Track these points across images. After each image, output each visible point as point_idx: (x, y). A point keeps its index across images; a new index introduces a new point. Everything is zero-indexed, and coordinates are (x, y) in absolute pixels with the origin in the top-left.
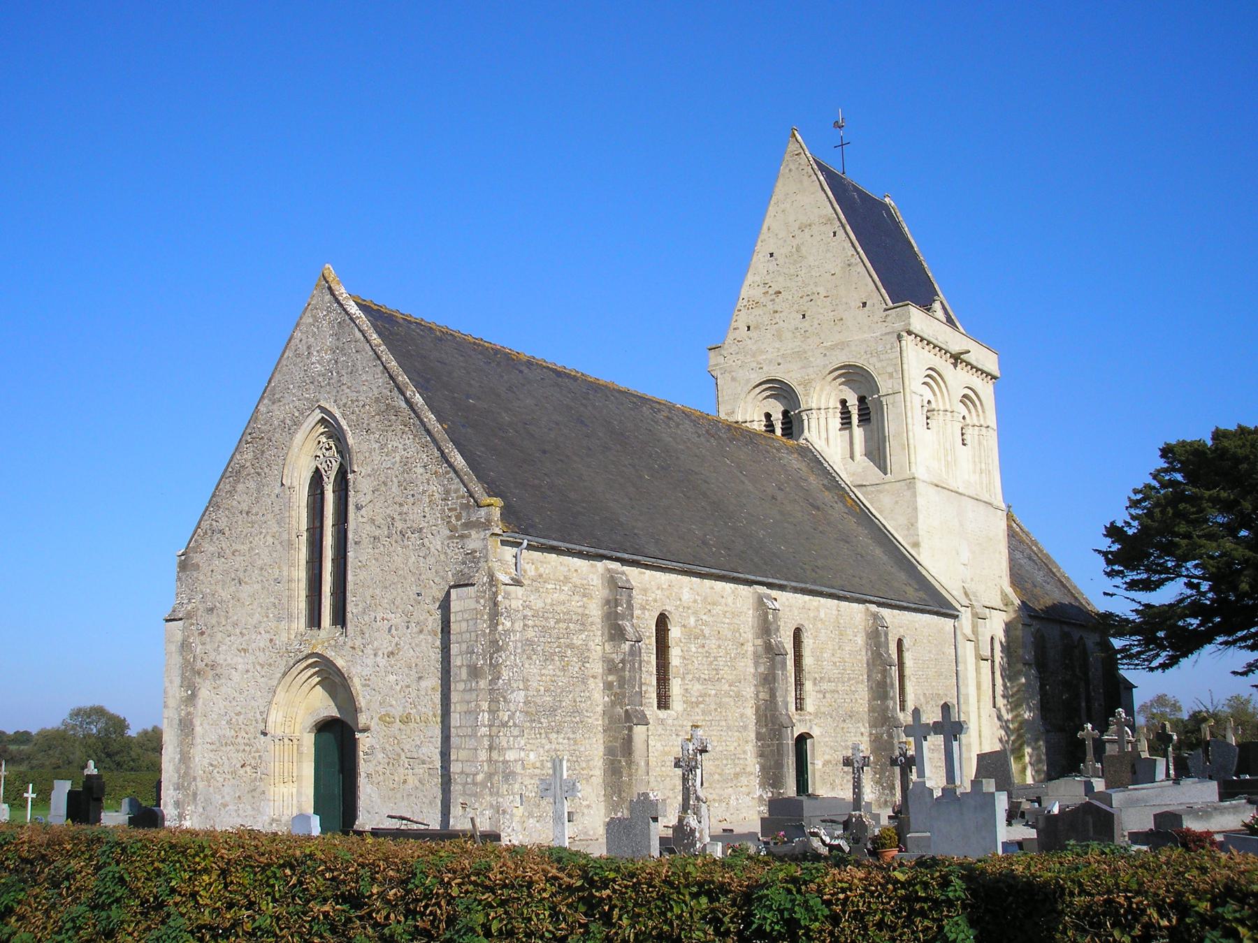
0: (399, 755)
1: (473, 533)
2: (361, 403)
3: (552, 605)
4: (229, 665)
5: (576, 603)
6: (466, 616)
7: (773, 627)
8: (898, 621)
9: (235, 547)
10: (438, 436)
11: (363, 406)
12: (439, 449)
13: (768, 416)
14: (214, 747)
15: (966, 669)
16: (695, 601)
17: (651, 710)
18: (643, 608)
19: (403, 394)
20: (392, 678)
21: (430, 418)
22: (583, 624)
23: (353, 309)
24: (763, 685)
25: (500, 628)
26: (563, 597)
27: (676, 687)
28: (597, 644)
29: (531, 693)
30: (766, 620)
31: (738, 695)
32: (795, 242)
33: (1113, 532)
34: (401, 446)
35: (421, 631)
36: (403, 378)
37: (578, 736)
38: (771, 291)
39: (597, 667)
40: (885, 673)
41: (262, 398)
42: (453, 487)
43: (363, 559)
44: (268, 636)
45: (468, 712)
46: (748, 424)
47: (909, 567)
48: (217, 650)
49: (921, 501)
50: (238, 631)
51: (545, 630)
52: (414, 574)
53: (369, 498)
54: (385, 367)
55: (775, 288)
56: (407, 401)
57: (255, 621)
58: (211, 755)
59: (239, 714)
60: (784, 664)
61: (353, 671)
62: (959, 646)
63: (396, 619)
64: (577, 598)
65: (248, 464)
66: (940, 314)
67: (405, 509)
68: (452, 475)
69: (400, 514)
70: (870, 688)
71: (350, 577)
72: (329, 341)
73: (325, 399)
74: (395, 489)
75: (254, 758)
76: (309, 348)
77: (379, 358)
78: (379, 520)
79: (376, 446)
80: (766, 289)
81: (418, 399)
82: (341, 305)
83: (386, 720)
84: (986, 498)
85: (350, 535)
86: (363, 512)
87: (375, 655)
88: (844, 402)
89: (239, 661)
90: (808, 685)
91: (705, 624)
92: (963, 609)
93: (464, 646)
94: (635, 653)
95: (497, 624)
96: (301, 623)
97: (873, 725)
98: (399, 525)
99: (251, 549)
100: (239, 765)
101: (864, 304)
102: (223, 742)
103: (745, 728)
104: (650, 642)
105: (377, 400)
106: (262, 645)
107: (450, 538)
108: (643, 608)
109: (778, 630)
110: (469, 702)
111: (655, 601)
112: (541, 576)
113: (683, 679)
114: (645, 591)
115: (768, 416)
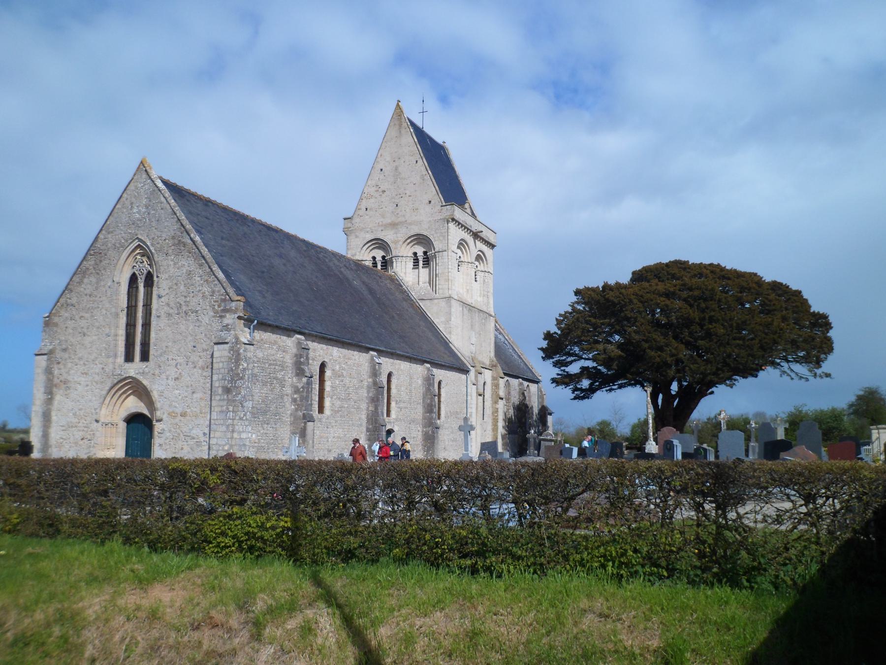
0: (179, 434)
1: (228, 315)
2: (164, 238)
3: (267, 356)
4: (75, 382)
5: (279, 356)
6: (223, 360)
7: (378, 373)
8: (440, 374)
9: (82, 314)
10: (209, 261)
11: (165, 240)
12: (210, 267)
13: (374, 258)
14: (64, 428)
15: (472, 399)
16: (339, 357)
17: (315, 413)
18: (313, 360)
19: (189, 235)
20: (177, 392)
21: (205, 251)
22: (282, 367)
23: (160, 184)
24: (371, 403)
25: (241, 367)
26: (273, 352)
27: (327, 403)
28: (290, 379)
29: (255, 402)
30: (374, 369)
31: (358, 408)
32: (395, 164)
33: (548, 336)
34: (186, 264)
35: (195, 367)
36: (189, 226)
37: (278, 426)
38: (380, 190)
39: (288, 390)
40: (432, 399)
41: (101, 230)
42: (217, 289)
43: (162, 325)
44: (101, 366)
45: (222, 412)
46: (363, 262)
47: (445, 343)
48: (68, 373)
49: (453, 310)
50: (82, 362)
51: (263, 369)
52: (192, 335)
53: (166, 292)
54: (179, 219)
55: (383, 188)
56: (191, 239)
57: (93, 357)
58: (62, 433)
59: (80, 410)
60: (382, 394)
61: (154, 387)
62: (469, 387)
63: (180, 360)
64: (280, 353)
65: (91, 267)
66: (468, 211)
67: (188, 299)
68: (216, 282)
69: (185, 302)
70: (424, 407)
71: (153, 335)
72: (144, 201)
73: (141, 234)
74: (182, 288)
75: (90, 434)
76: (132, 204)
77: (175, 214)
78: (172, 304)
79: (172, 263)
80: (377, 189)
81: (197, 238)
82: (153, 181)
83: (172, 415)
84: (485, 309)
85: (154, 312)
86: (163, 299)
87: (167, 379)
88: (415, 254)
89: (82, 379)
90: (393, 404)
91: (344, 369)
92: (471, 368)
93: (221, 376)
94: (309, 384)
95: (239, 365)
96: (121, 359)
97: (424, 426)
98: (184, 308)
99: (92, 316)
100: (80, 438)
101: (430, 202)
102: (70, 426)
103: (361, 425)
104: (316, 378)
105: (173, 238)
106: (97, 371)
107: (214, 317)
108: (313, 360)
109: (380, 374)
110: (222, 406)
111: (320, 356)
112: (262, 340)
113: (332, 398)
114: (315, 350)
115: (374, 258)
